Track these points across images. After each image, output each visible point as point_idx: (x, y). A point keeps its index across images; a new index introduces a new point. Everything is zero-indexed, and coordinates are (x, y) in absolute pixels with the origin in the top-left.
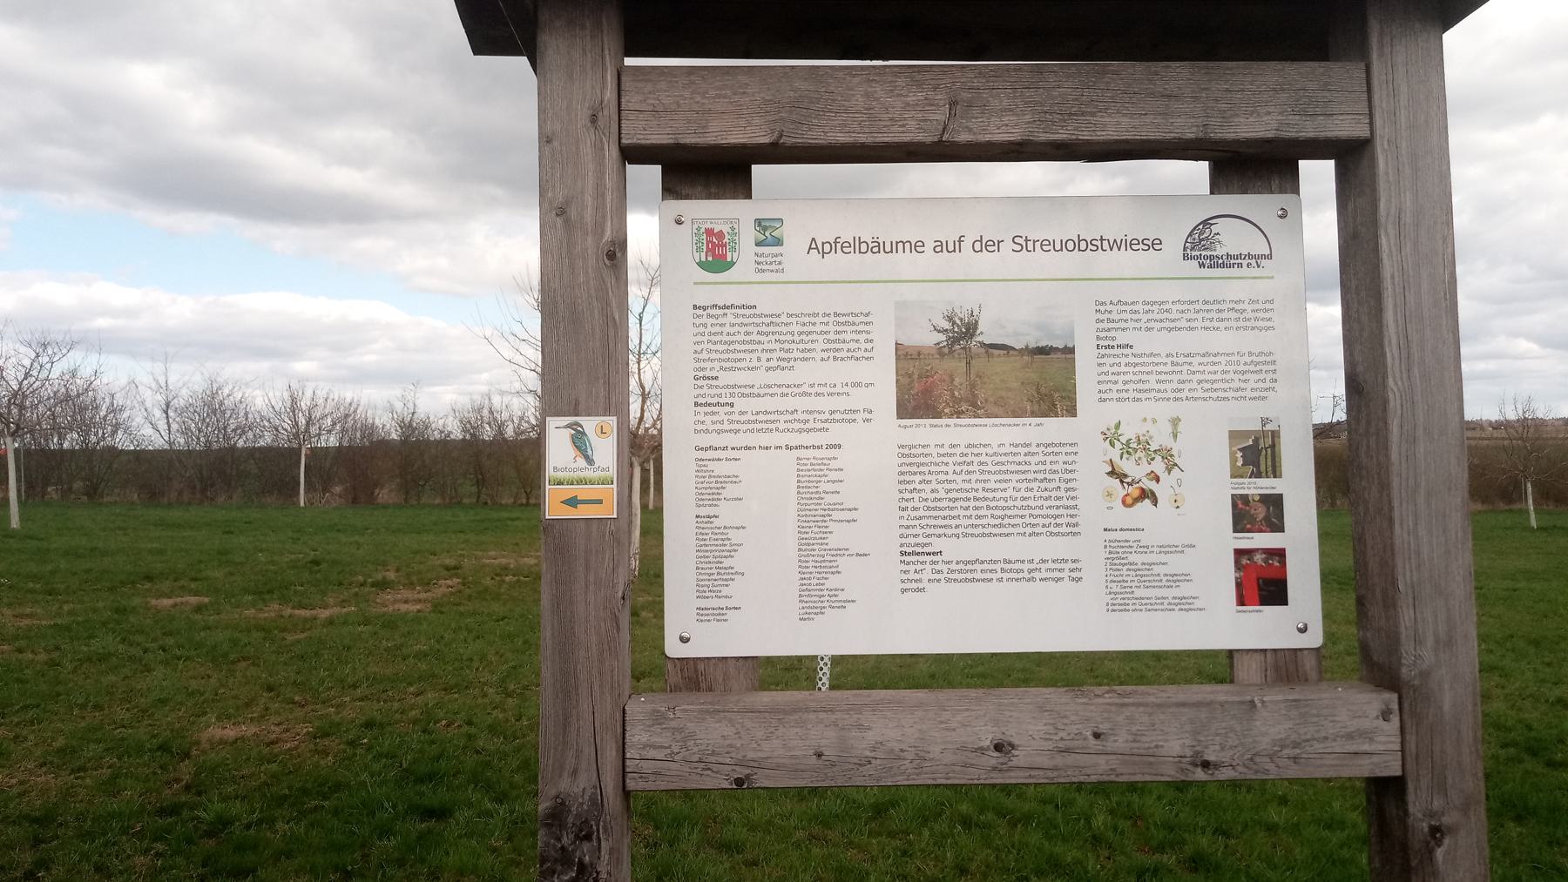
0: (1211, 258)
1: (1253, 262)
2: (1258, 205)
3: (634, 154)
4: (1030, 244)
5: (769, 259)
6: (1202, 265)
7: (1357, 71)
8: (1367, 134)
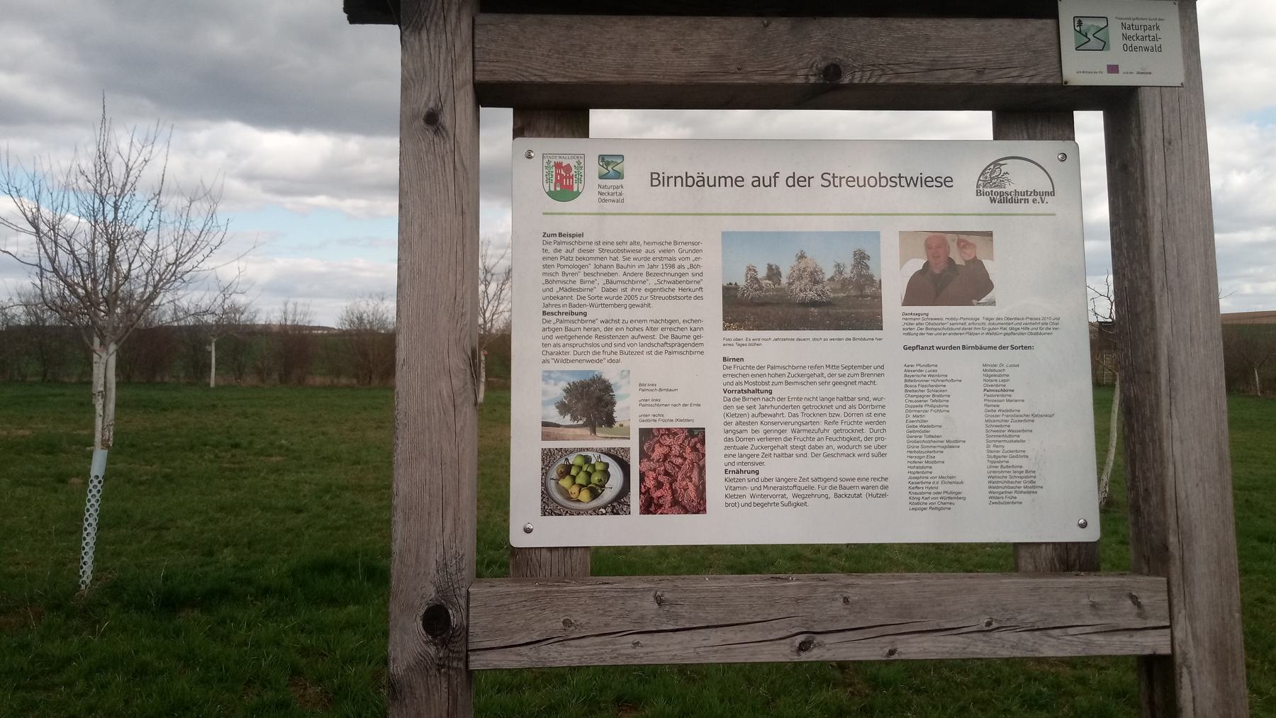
0: (1001, 194)
1: (1038, 198)
2: (1043, 149)
3: (487, 95)
4: (837, 181)
5: (611, 190)
6: (993, 201)
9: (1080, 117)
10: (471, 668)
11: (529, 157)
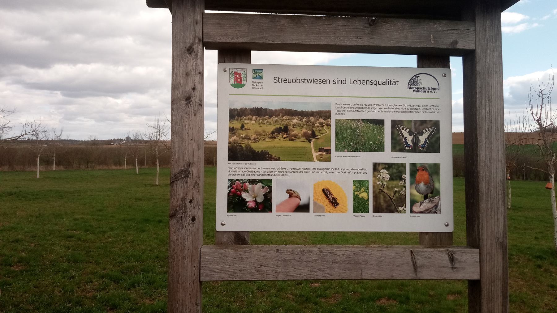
0: (418, 88)
2: (437, 72)
3: (209, 46)
4: (280, 80)
5: (258, 84)
6: (414, 91)
7: (473, 28)
8: (474, 48)
9: (452, 59)
10: (201, 280)
11: (225, 71)
